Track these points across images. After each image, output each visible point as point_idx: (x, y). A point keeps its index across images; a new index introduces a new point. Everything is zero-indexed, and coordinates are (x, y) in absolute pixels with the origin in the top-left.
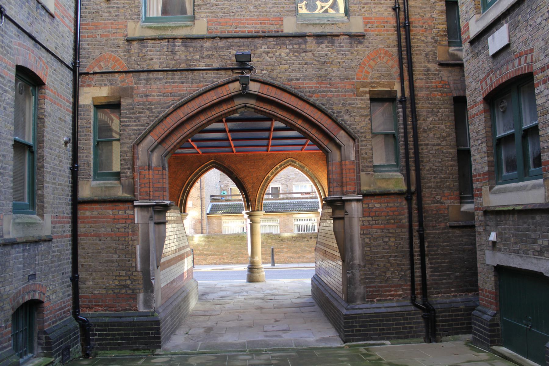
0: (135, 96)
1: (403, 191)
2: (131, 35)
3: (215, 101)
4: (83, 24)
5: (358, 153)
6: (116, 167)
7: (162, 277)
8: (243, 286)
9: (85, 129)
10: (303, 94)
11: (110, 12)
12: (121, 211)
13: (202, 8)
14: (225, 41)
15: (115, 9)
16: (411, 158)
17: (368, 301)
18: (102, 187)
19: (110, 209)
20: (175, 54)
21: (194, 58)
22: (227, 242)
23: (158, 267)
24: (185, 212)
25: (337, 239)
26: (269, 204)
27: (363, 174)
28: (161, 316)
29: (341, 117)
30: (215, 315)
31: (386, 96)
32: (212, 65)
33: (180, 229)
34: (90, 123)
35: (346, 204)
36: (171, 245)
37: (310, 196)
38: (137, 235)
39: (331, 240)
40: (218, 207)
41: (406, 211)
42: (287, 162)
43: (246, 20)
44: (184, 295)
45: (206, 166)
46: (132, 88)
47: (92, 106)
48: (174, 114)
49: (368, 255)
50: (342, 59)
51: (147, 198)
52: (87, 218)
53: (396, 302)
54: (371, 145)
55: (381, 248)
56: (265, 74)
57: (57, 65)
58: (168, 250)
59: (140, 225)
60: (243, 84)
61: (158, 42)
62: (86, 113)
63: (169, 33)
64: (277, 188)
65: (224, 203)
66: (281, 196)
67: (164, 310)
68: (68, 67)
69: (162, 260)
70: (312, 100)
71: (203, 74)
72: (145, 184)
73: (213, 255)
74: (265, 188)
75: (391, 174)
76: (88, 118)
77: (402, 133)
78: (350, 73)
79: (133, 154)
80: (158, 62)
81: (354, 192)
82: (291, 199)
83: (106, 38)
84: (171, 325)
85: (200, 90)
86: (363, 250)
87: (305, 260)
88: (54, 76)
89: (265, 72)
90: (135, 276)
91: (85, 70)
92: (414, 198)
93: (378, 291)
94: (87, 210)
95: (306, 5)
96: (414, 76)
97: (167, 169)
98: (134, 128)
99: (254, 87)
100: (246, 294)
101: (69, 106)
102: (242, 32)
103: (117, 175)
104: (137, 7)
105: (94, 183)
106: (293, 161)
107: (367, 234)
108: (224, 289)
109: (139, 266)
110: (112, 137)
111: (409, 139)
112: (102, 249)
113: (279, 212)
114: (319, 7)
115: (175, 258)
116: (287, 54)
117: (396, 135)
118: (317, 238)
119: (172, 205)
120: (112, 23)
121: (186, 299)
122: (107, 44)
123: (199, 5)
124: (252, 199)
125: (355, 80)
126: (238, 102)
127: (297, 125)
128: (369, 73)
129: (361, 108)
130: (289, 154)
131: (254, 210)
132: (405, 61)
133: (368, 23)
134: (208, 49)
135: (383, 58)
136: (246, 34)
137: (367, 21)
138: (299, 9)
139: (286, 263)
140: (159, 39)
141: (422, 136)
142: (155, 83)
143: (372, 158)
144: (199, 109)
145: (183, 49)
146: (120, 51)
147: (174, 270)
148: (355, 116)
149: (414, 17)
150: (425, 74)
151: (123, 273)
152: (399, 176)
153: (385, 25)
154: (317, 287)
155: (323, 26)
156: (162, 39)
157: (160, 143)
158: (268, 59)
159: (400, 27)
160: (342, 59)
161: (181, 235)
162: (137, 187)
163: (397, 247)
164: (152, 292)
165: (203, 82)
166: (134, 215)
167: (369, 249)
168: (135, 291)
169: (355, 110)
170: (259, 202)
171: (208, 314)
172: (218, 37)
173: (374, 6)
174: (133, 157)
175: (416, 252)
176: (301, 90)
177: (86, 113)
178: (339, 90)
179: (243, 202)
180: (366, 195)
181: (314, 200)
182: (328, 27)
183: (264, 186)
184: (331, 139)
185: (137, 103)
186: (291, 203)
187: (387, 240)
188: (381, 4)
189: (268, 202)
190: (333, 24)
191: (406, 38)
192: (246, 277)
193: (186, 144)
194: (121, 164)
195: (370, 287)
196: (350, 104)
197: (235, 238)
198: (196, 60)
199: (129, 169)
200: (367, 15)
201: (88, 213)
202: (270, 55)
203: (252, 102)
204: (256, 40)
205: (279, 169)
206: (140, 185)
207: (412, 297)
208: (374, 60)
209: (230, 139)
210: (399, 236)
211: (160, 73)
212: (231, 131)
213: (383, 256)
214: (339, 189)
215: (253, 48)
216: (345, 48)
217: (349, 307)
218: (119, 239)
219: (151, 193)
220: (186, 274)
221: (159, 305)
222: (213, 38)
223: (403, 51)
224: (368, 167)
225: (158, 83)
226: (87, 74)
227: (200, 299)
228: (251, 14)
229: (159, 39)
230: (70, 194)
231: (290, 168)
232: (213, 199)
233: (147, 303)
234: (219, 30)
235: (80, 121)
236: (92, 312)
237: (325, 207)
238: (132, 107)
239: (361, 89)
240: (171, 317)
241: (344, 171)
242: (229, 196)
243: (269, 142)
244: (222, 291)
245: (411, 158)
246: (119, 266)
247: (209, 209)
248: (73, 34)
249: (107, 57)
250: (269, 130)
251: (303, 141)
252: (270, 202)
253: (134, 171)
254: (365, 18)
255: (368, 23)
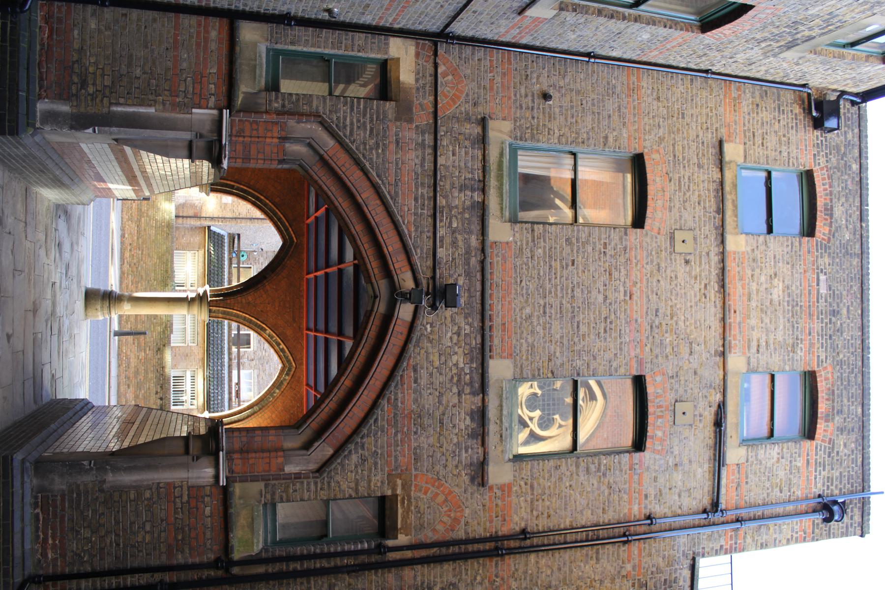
0: (398, 123)
1: (232, 552)
2: (491, 124)
3: (385, 249)
4: (509, 55)
5: (295, 478)
6: (287, 86)
7: (98, 146)
8: (79, 282)
9: (350, 42)
10: (392, 388)
11: (526, 96)
12: (214, 87)
13: (529, 236)
14: (479, 268)
15: (530, 105)
16: (287, 566)
17: (36, 497)
18: (255, 60)
19: (219, 69)
20: (460, 191)
21: (454, 219)
22: (159, 258)
23: (116, 140)
24: (213, 190)
25: (153, 442)
26: (223, 329)
27: (261, 485)
28: (27, 138)
29: (356, 449)
30: (26, 231)
31: (388, 523)
32: (442, 247)
33: (182, 181)
34: (359, 51)
35: (212, 458)
36: (154, 165)
37: (234, 398)
38: (173, 110)
39: (152, 433)
40: (219, 246)
41: (197, 560)
42: (288, 361)
43: (509, 302)
44: (65, 179)
45: (287, 230)
46: (410, 120)
47: (386, 57)
48: (368, 183)
49: (120, 497)
50: (447, 450)
51: (234, 132)
52: (207, 32)
53: (32, 549)
54: (309, 499)
55: (133, 519)
56: (426, 329)
57: (450, 10)
58: (146, 160)
59: (189, 116)
60: (410, 294)
61: (480, 165)
62: (375, 46)
63: (492, 182)
64: (249, 343)
65: (226, 256)
66: (234, 349)
67: (38, 144)
68: (448, 25)
69: (128, 150)
70: (384, 402)
71: (428, 232)
72: (257, 130)
73: (139, 232)
74: (247, 324)
75: (261, 533)
76: (370, 50)
77: (329, 549)
78: (426, 464)
79: (307, 115)
80: (449, 163)
81: (231, 471)
82: (230, 366)
83: (488, 86)
84: (10, 155)
85: (404, 227)
86: (131, 487)
87: (122, 388)
88: (433, 4)
89: (429, 329)
90: (102, 101)
91: (441, 51)
92: (220, 573)
93: (55, 514)
94: (219, 33)
95: (535, 394)
96: (419, 567)
97: (280, 166)
98: (348, 119)
99: (405, 311)
100: (63, 285)
101: (386, 21)
102: (491, 295)
103: (273, 86)
104: (533, 137)
105: (263, 48)
106: (290, 370)
107: (158, 493)
108: (75, 247)
109: (120, 109)
110: (338, 82)
111: (318, 561)
112: (152, 51)
113: (208, 346)
114: (532, 414)
115: (131, 169)
116: (456, 365)
117: (325, 539)
118: (161, 409)
119: (220, 172)
120: (510, 98)
121: (57, 183)
122: (479, 88)
123: (533, 230)
124: (229, 301)
125: (414, 472)
126: (382, 286)
127: (344, 378)
128: (425, 493)
129: (369, 481)
130: (301, 364)
131: (210, 304)
132: (444, 551)
133: (503, 491)
134: (467, 241)
135: (449, 516)
136: (488, 302)
137: (506, 489)
138: (530, 383)
139: (119, 355)
140: (484, 167)
141: (323, 582)
142: (417, 157)
143: (288, 501)
144: (373, 223)
145: (468, 203)
146: (469, 107)
147: (110, 166)
148: (357, 472)
149: (512, 563)
150: (423, 583)
151: (108, 82)
152: (258, 546)
153: (500, 518)
154: (69, 409)
155: (498, 422)
156: (484, 171)
157: (322, 159)
158: (449, 334)
159: (496, 541)
160: (447, 450)
161: (171, 183)
162: (253, 117)
163: (133, 546)
164: (72, 128)
165: (416, 231)
166: (207, 108)
167: (132, 497)
168: (74, 98)
169: (365, 473)
170: (224, 313)
171: (29, 219)
172: (485, 258)
173: (529, 499)
174: (302, 115)
175: (125, 580)
176: (400, 386)
177: (375, 46)
178: (398, 446)
179: (226, 286)
180: (226, 492)
181: (226, 404)
182: (497, 428)
183: (250, 321)
184: (319, 434)
185: (388, 127)
186: (222, 365)
187: (148, 528)
188: (532, 511)
189: (226, 327)
190: (501, 436)
191: (479, 552)
192: (96, 287)
193: (321, 200)
194: (291, 94)
195: (63, 500)
196: (376, 464)
197: (167, 271)
198: (451, 223)
199: (283, 106)
200: (514, 489)
201: (214, 34)
202: (455, 337)
203: (381, 307)
204: (479, 317)
205: (277, 348)
206: (256, 122)
207: (40, 576)
208: (446, 501)
209: (328, 270)
210: (155, 548)
211: (432, 165)
212: (340, 271)
213: (119, 523)
214: (237, 446)
215: (466, 311)
216: (464, 455)
217: (28, 464)
218: (166, 80)
219: (241, 139)
220: (103, 185)
221: (47, 136)
222: (483, 250)
223: (460, 548)
224: (273, 494)
225: (417, 161)
226: (436, 54)
227: (58, 206)
228: (518, 310)
229: (484, 167)
230: (247, 9)
231: (280, 366)
232: (234, 238)
233: (52, 118)
234: (495, 259)
235: (363, 36)
236: (40, 22)
237: (210, 424)
238: (381, 118)
239: (399, 482)
240: (24, 155)
241: (266, 455)
242: (239, 263)
243: (321, 332)
244: (72, 245)
245: (287, 566)
246: (121, 76)
247: (217, 230)
248: (495, 38)
249: (459, 86)
250: (340, 333)
251: (322, 389)
252: (226, 331)
253: (279, 113)
254: (510, 486)
255: (503, 491)
